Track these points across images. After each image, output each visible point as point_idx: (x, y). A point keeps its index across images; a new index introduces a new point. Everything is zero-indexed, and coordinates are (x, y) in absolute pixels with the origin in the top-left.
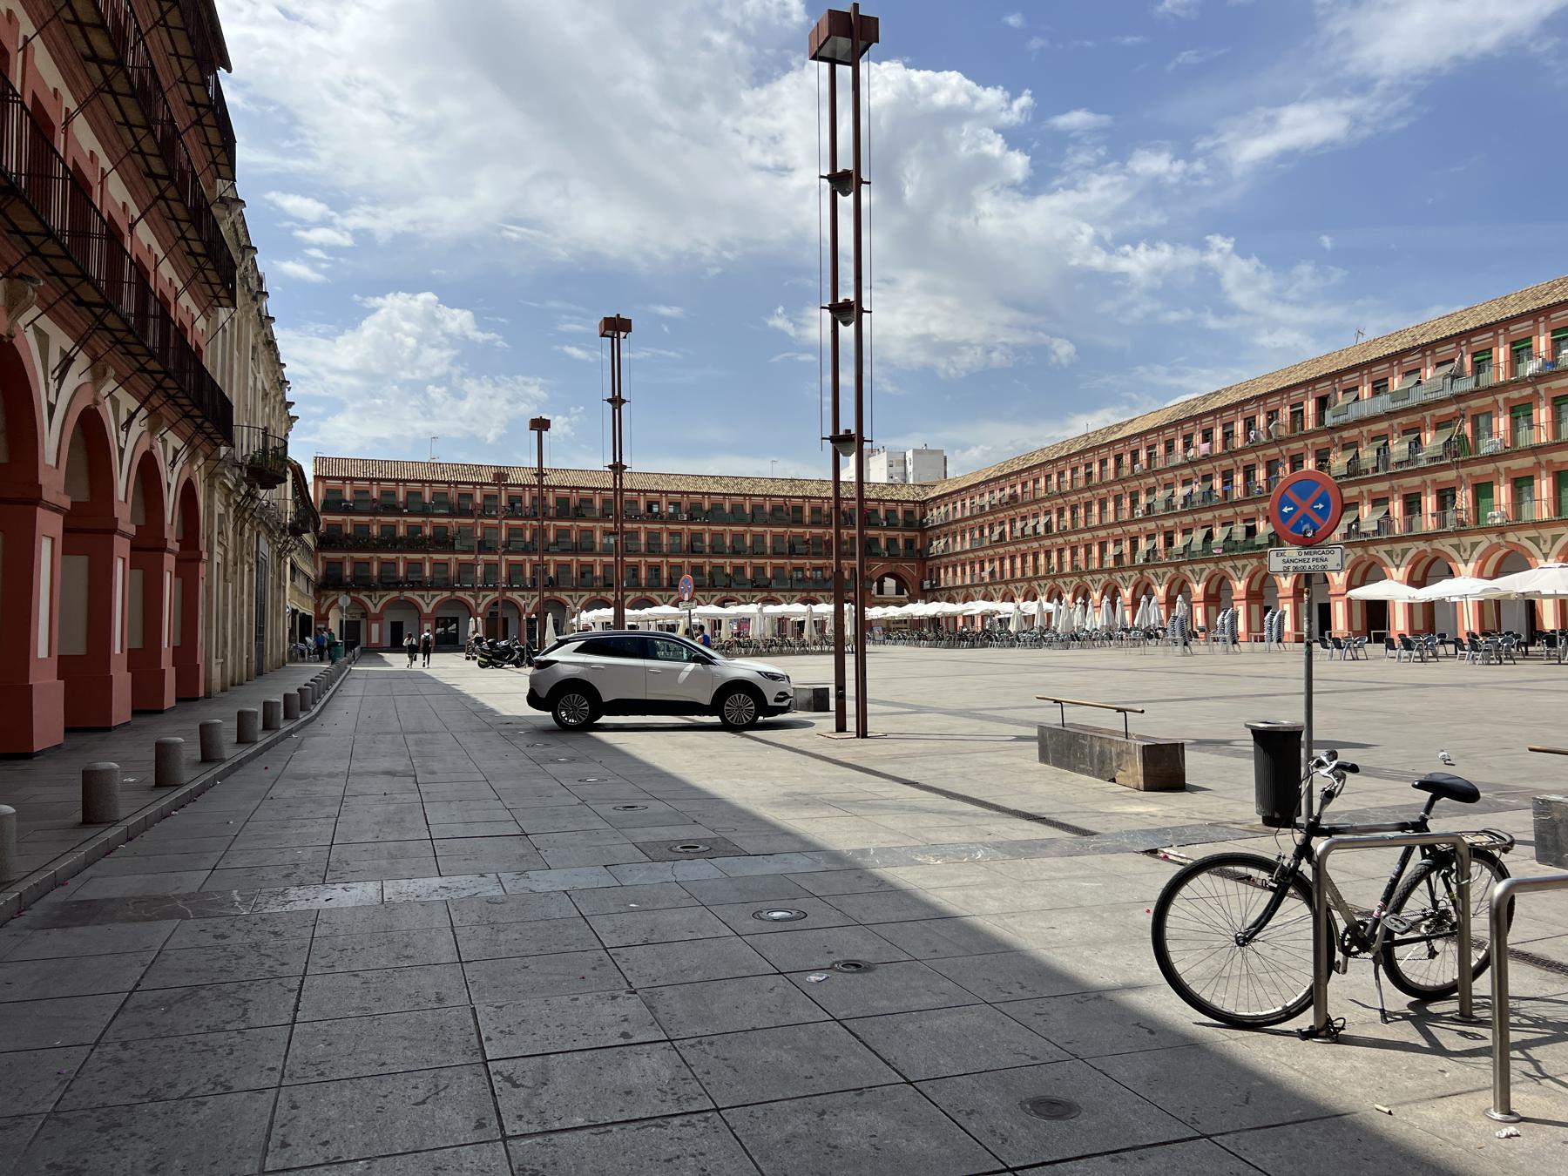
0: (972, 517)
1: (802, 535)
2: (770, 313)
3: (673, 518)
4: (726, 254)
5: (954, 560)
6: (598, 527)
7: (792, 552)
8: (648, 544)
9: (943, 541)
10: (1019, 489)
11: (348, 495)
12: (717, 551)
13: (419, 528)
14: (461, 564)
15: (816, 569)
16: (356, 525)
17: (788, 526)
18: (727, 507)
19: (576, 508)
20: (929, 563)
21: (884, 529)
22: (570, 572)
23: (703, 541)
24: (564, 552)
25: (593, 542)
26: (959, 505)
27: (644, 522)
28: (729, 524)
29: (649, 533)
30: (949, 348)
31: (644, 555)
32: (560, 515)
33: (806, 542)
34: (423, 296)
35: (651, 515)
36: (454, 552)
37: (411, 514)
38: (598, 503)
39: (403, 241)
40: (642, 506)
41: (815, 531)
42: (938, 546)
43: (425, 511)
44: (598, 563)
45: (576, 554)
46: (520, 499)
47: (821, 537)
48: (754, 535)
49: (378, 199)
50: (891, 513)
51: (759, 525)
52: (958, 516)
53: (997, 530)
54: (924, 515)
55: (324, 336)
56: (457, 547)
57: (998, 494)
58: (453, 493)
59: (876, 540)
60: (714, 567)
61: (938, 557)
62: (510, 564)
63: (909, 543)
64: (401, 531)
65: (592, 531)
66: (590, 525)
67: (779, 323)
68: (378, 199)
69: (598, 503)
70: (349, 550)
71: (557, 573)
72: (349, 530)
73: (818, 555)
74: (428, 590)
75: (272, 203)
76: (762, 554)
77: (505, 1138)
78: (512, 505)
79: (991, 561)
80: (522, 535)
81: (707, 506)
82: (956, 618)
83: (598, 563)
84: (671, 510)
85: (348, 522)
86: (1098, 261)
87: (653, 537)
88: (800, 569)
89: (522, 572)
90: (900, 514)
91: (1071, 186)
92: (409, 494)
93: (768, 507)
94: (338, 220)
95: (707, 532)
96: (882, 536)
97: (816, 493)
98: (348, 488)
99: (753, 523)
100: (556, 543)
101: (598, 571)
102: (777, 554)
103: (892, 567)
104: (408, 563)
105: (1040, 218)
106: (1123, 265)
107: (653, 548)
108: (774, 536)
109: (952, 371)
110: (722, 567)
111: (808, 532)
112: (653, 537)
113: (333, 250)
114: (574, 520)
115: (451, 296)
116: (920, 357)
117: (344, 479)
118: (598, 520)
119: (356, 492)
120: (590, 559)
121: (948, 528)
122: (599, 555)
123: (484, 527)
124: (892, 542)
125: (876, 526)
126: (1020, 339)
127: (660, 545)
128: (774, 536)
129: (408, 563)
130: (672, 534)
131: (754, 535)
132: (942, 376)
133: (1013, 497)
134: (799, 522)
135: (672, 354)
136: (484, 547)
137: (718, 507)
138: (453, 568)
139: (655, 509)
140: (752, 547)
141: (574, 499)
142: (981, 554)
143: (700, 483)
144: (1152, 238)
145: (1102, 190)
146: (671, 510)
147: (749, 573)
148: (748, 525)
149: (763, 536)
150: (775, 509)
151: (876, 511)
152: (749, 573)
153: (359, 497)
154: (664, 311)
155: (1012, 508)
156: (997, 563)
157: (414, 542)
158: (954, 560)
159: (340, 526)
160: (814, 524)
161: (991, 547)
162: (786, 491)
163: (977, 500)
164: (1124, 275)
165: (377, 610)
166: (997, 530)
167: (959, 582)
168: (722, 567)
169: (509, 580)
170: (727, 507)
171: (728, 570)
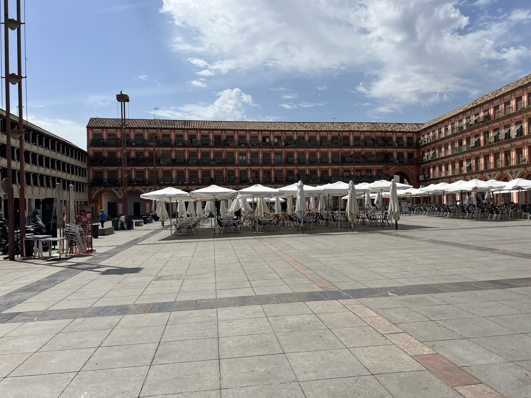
0: (454, 135)
1: (349, 152)
2: (358, 85)
3: (277, 145)
4: (342, 68)
5: (438, 162)
6: (237, 151)
7: (343, 161)
8: (263, 159)
9: (431, 153)
10: (491, 111)
11: (105, 136)
12: (301, 162)
13: (142, 153)
14: (164, 172)
15: (357, 170)
16: (110, 153)
17: (341, 147)
18: (307, 138)
19: (225, 141)
20: (423, 166)
21: (396, 147)
22: (222, 175)
23: (293, 157)
24: (218, 164)
25: (234, 159)
26: (443, 130)
27: (261, 148)
28: (307, 147)
29: (264, 153)
30: (427, 96)
31: (262, 165)
32: (216, 145)
33: (351, 156)
34: (235, 90)
35: (265, 143)
36: (161, 165)
37: (137, 145)
38: (236, 138)
39: (231, 72)
40: (260, 139)
41: (356, 150)
42: (428, 155)
43: (144, 144)
44: (237, 170)
45: (225, 166)
46: (195, 137)
47: (359, 153)
48: (322, 153)
49: (222, 57)
50: (399, 139)
51: (324, 147)
52: (443, 136)
53: (473, 141)
54: (419, 139)
55: (203, 106)
56: (162, 163)
57: (473, 118)
58: (160, 134)
59: (391, 154)
60: (300, 171)
61: (429, 162)
62: (190, 172)
63: (410, 155)
64: (133, 155)
65: (233, 153)
66: (232, 150)
67: (361, 89)
68: (222, 57)
69: (236, 138)
70: (105, 165)
71: (215, 175)
72: (106, 155)
73: (358, 163)
74: (147, 185)
75: (189, 62)
76: (326, 163)
77: (219, 360)
78: (191, 140)
79: (468, 160)
80: (196, 156)
81: (295, 137)
82: (440, 197)
83: (237, 170)
84: (276, 141)
85: (105, 151)
86: (494, 55)
87: (266, 156)
88: (348, 171)
89: (197, 176)
90: (405, 139)
91: (483, 28)
92: (137, 135)
93: (329, 137)
94: (210, 67)
95: (296, 152)
96: (395, 152)
97: (356, 129)
98: (105, 132)
99: (321, 146)
100: (214, 160)
101: (237, 175)
102: (334, 163)
103: (401, 169)
104: (137, 172)
105: (469, 41)
106: (505, 56)
107: (266, 161)
108: (333, 153)
109: (427, 104)
110: (304, 171)
111: (352, 151)
112: (266, 156)
113: (208, 78)
114: (224, 147)
115: (246, 90)
116: (414, 99)
117: (103, 128)
118: (236, 147)
119: (109, 135)
120: (233, 168)
121: (435, 144)
122: (237, 166)
123: (176, 152)
124: (400, 155)
125: (391, 146)
126: (457, 88)
127: (270, 159)
128: (333, 153)
129: (137, 172)
130: (276, 154)
131: (322, 153)
132: (423, 106)
133: (487, 117)
134: (347, 145)
135: (321, 104)
136: (174, 163)
137: (301, 138)
138: (160, 174)
139: (267, 140)
140: (321, 159)
141: (224, 136)
142: (461, 157)
143: (292, 125)
144: (516, 46)
145: (496, 29)
146: (276, 141)
147: (319, 174)
148: (318, 147)
149: (327, 153)
150: (333, 138)
151: (391, 138)
152: (319, 174)
153: (111, 137)
154: (320, 89)
155: (487, 124)
156: (473, 162)
157: (139, 160)
158: (438, 162)
159: (100, 153)
160: (356, 146)
161: (469, 151)
162: (340, 128)
163: (457, 124)
164: (505, 60)
165: (121, 197)
166: (473, 141)
167: (443, 175)
168: (304, 171)
169: (190, 180)
170: (307, 138)
171: (307, 172)
